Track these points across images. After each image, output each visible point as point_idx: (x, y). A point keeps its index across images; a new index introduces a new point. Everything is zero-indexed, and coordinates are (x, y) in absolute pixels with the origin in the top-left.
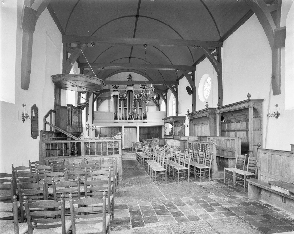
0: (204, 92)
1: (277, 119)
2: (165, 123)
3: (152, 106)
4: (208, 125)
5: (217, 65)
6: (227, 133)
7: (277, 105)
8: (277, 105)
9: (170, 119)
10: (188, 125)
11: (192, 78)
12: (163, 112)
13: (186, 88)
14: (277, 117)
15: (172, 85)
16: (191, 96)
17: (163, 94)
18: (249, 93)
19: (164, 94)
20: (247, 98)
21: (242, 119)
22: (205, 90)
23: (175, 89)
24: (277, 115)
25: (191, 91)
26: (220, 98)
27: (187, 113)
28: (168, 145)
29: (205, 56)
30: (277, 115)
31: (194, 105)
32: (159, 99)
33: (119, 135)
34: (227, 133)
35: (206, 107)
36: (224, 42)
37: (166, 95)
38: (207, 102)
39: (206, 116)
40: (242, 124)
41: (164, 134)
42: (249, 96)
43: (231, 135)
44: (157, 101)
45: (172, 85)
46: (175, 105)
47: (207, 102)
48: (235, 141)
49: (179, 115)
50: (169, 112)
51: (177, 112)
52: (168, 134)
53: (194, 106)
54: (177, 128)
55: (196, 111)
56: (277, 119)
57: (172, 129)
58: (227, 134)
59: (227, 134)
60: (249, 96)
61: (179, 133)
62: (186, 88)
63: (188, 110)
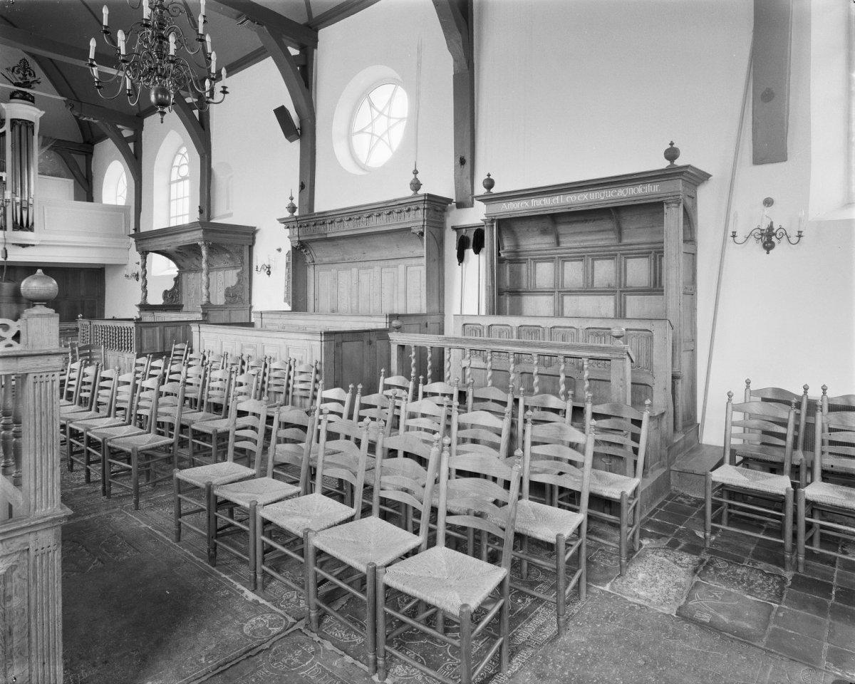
0: (355, 139)
1: (768, 253)
2: (147, 252)
3: (52, 175)
4: (396, 266)
5: (200, 131)
6: (508, 302)
7: (768, 202)
8: (768, 202)
9: (183, 235)
10: (137, 275)
11: (198, 118)
12: (116, 209)
13: (276, 111)
14: (769, 246)
15: (119, 126)
16: (296, 144)
17: (120, 130)
18: (674, 142)
19: (127, 133)
20: (665, 164)
21: (597, 249)
22: (361, 131)
23: (196, 112)
24: (768, 239)
25: (299, 126)
26: (466, 160)
27: (287, 214)
28: (217, 351)
29: (265, 53)
30: (768, 239)
31: (307, 185)
32: (92, 154)
33: (32, 302)
34: (508, 302)
35: (410, 193)
36: (95, 146)
37: (137, 139)
38: (416, 172)
39: (409, 229)
40: (593, 267)
41: (139, 301)
42: (672, 154)
43: (567, 311)
44: (81, 160)
45: (119, 126)
46: (187, 182)
47: (416, 172)
48: (651, 337)
49: (8, 260)
50: (151, 212)
51: (206, 205)
52: (160, 301)
53: (206, 212)
54: (192, 276)
55: (316, 211)
56: (768, 253)
57: (176, 279)
58: (508, 306)
59: (508, 306)
60: (672, 154)
61: (226, 296)
62: (276, 111)
63: (413, 176)
